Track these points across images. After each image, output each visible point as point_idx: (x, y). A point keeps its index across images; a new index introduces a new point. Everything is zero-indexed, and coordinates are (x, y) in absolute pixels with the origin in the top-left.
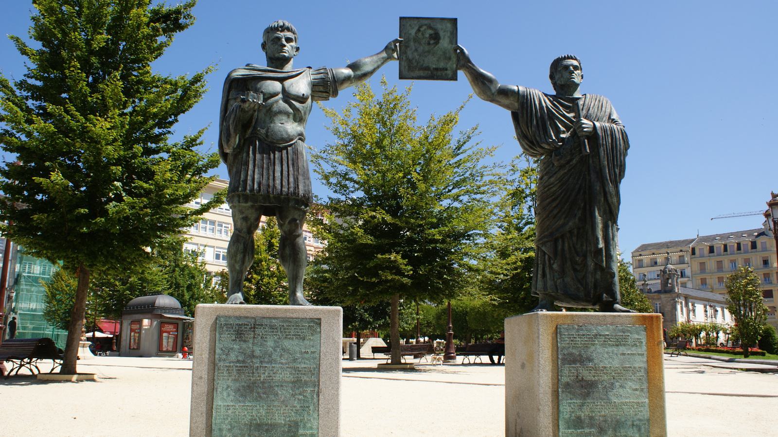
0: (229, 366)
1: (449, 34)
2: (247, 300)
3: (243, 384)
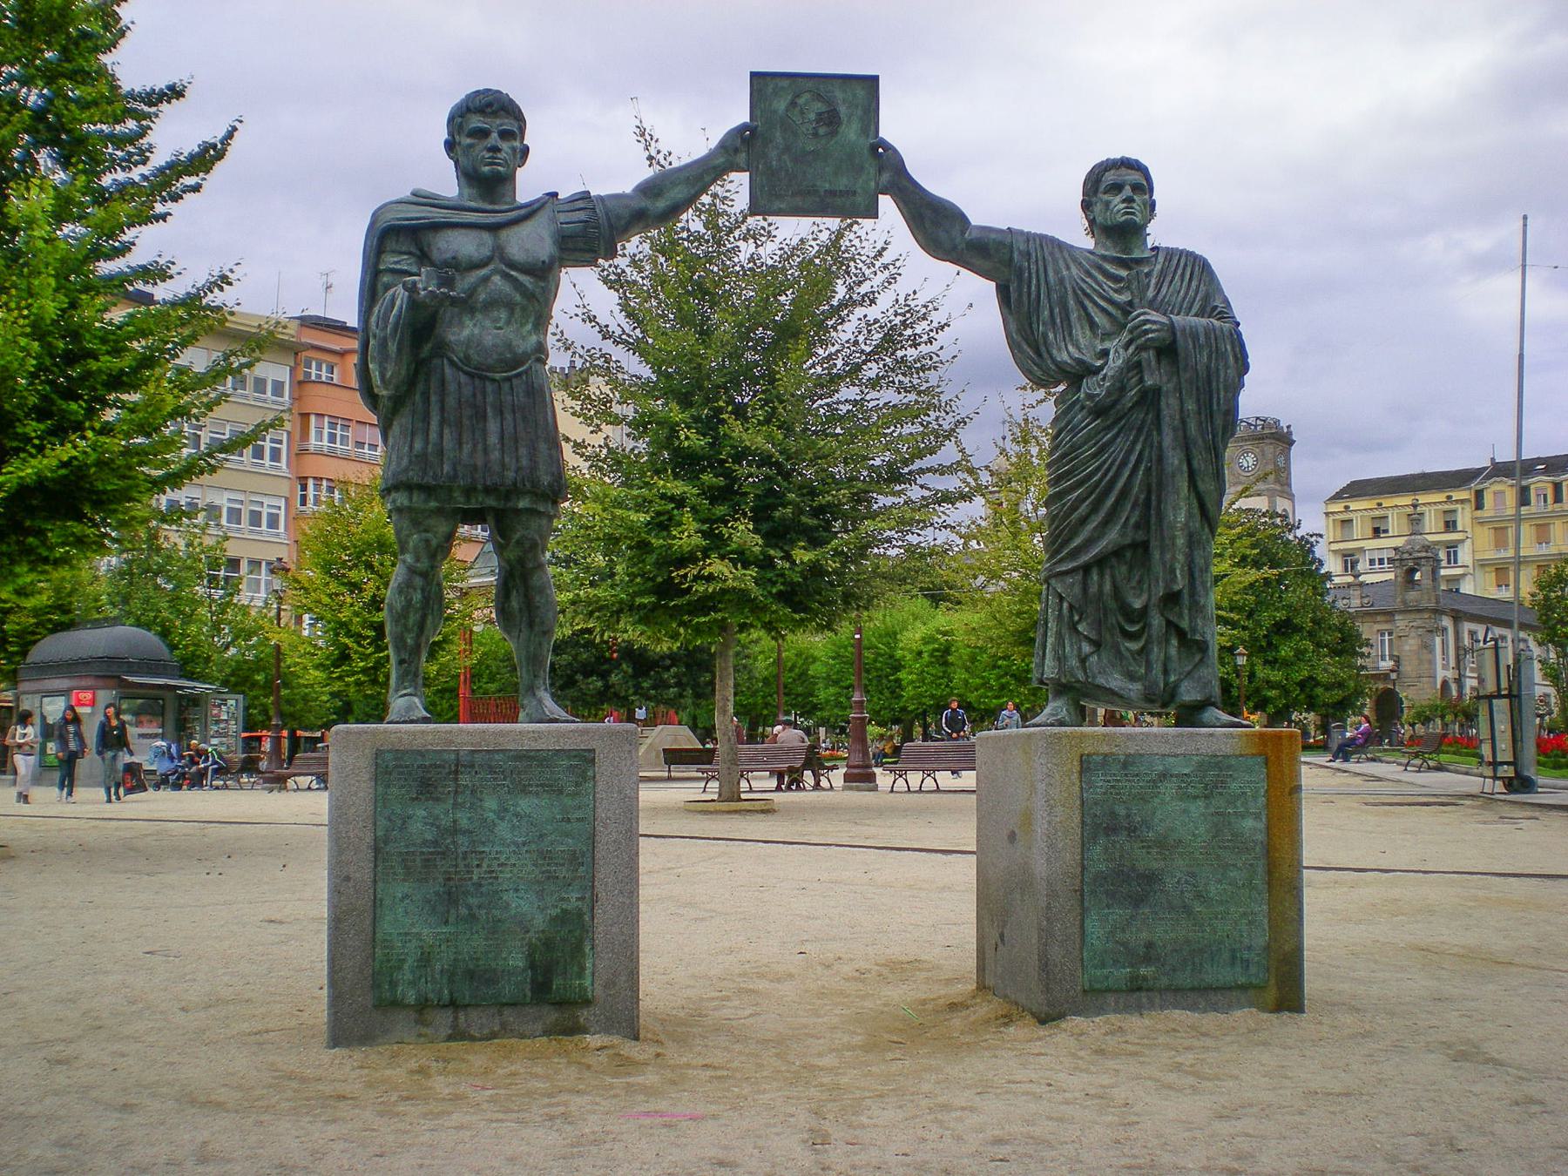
1: (859, 112)
2: (436, 714)
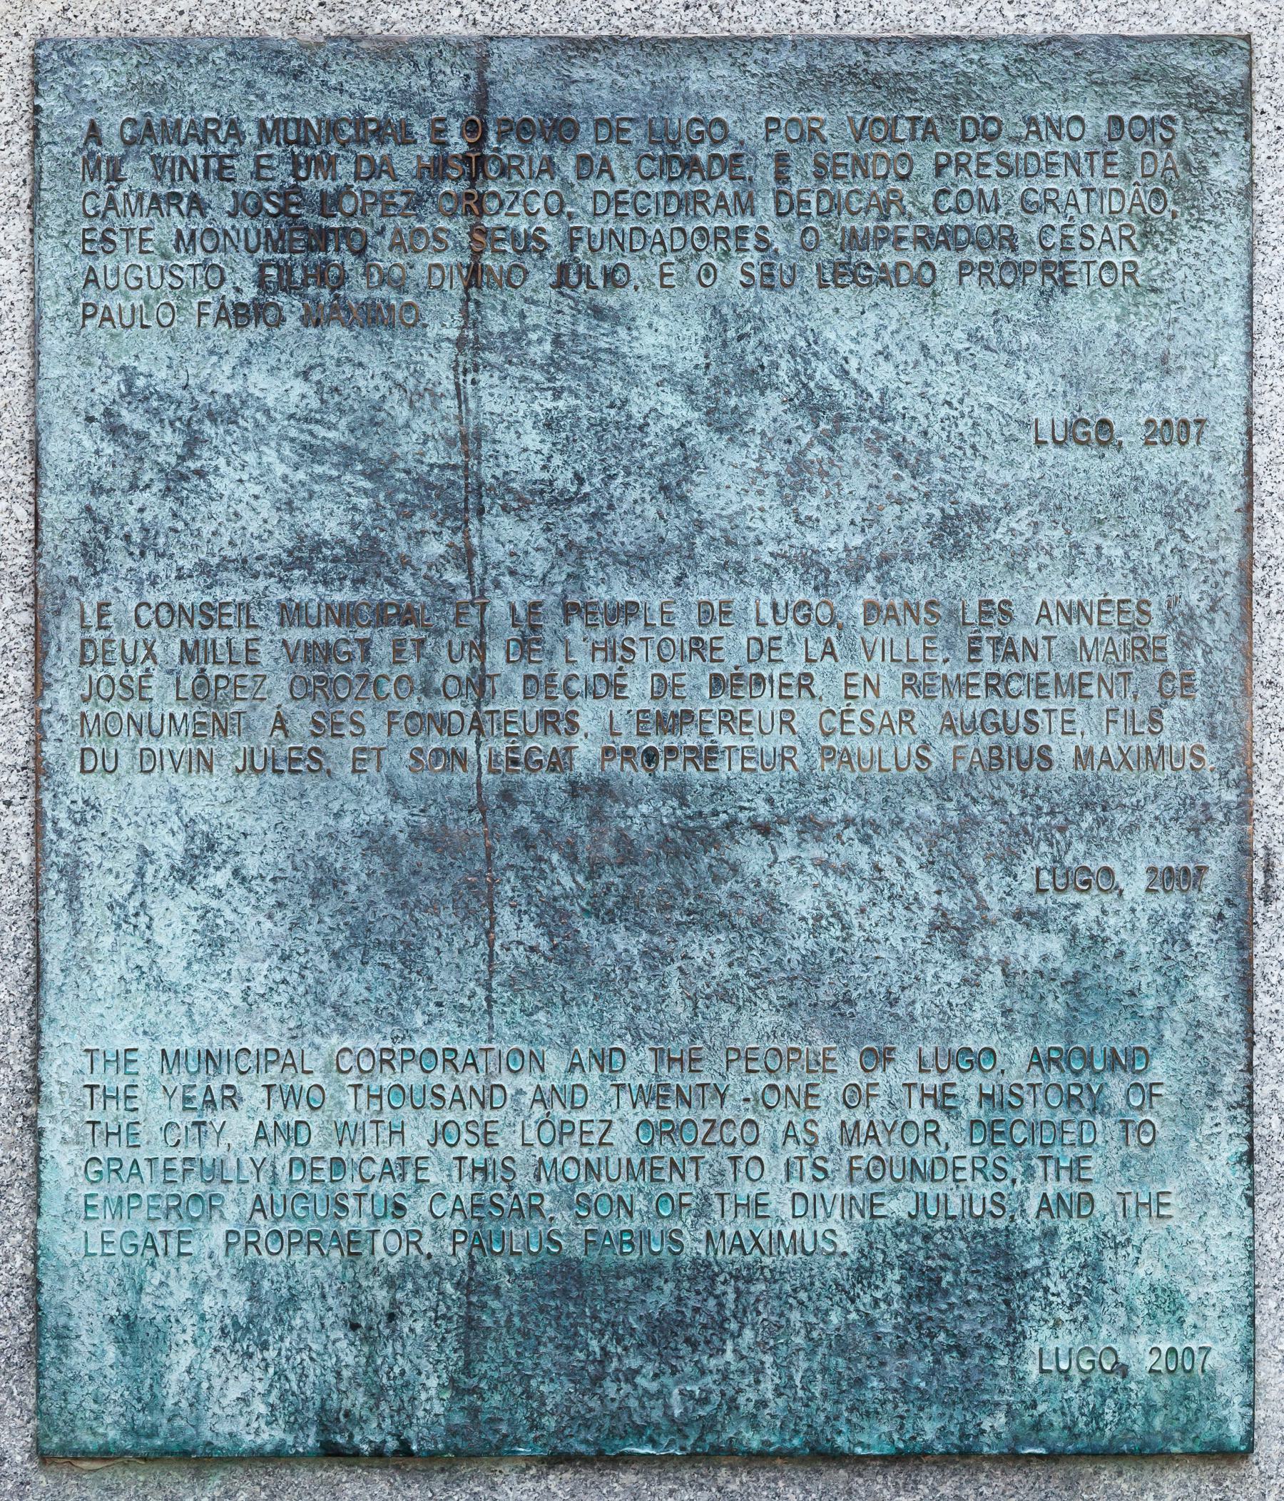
0: (210, 614)
3: (376, 807)
